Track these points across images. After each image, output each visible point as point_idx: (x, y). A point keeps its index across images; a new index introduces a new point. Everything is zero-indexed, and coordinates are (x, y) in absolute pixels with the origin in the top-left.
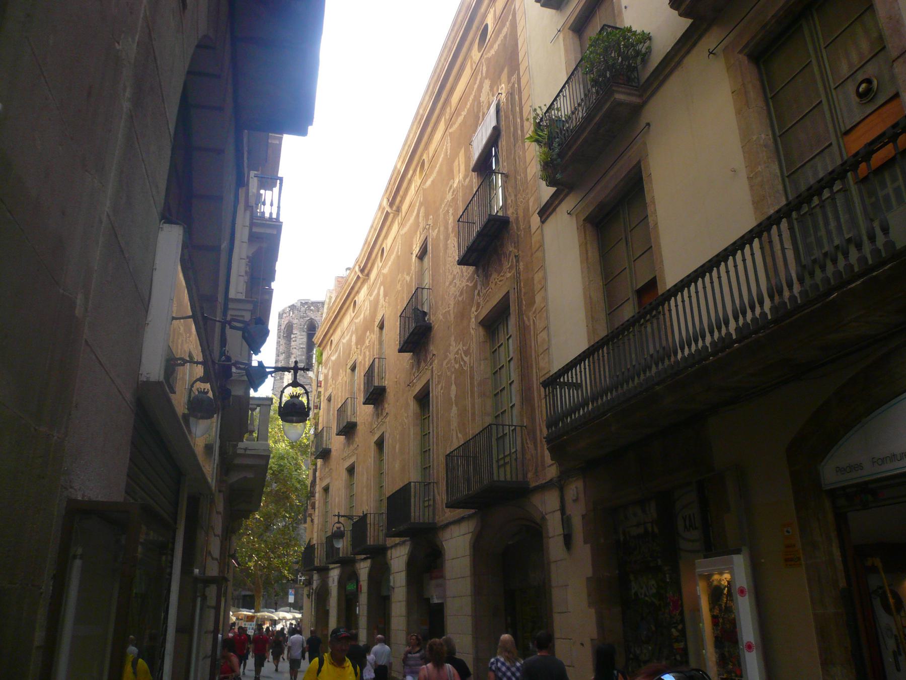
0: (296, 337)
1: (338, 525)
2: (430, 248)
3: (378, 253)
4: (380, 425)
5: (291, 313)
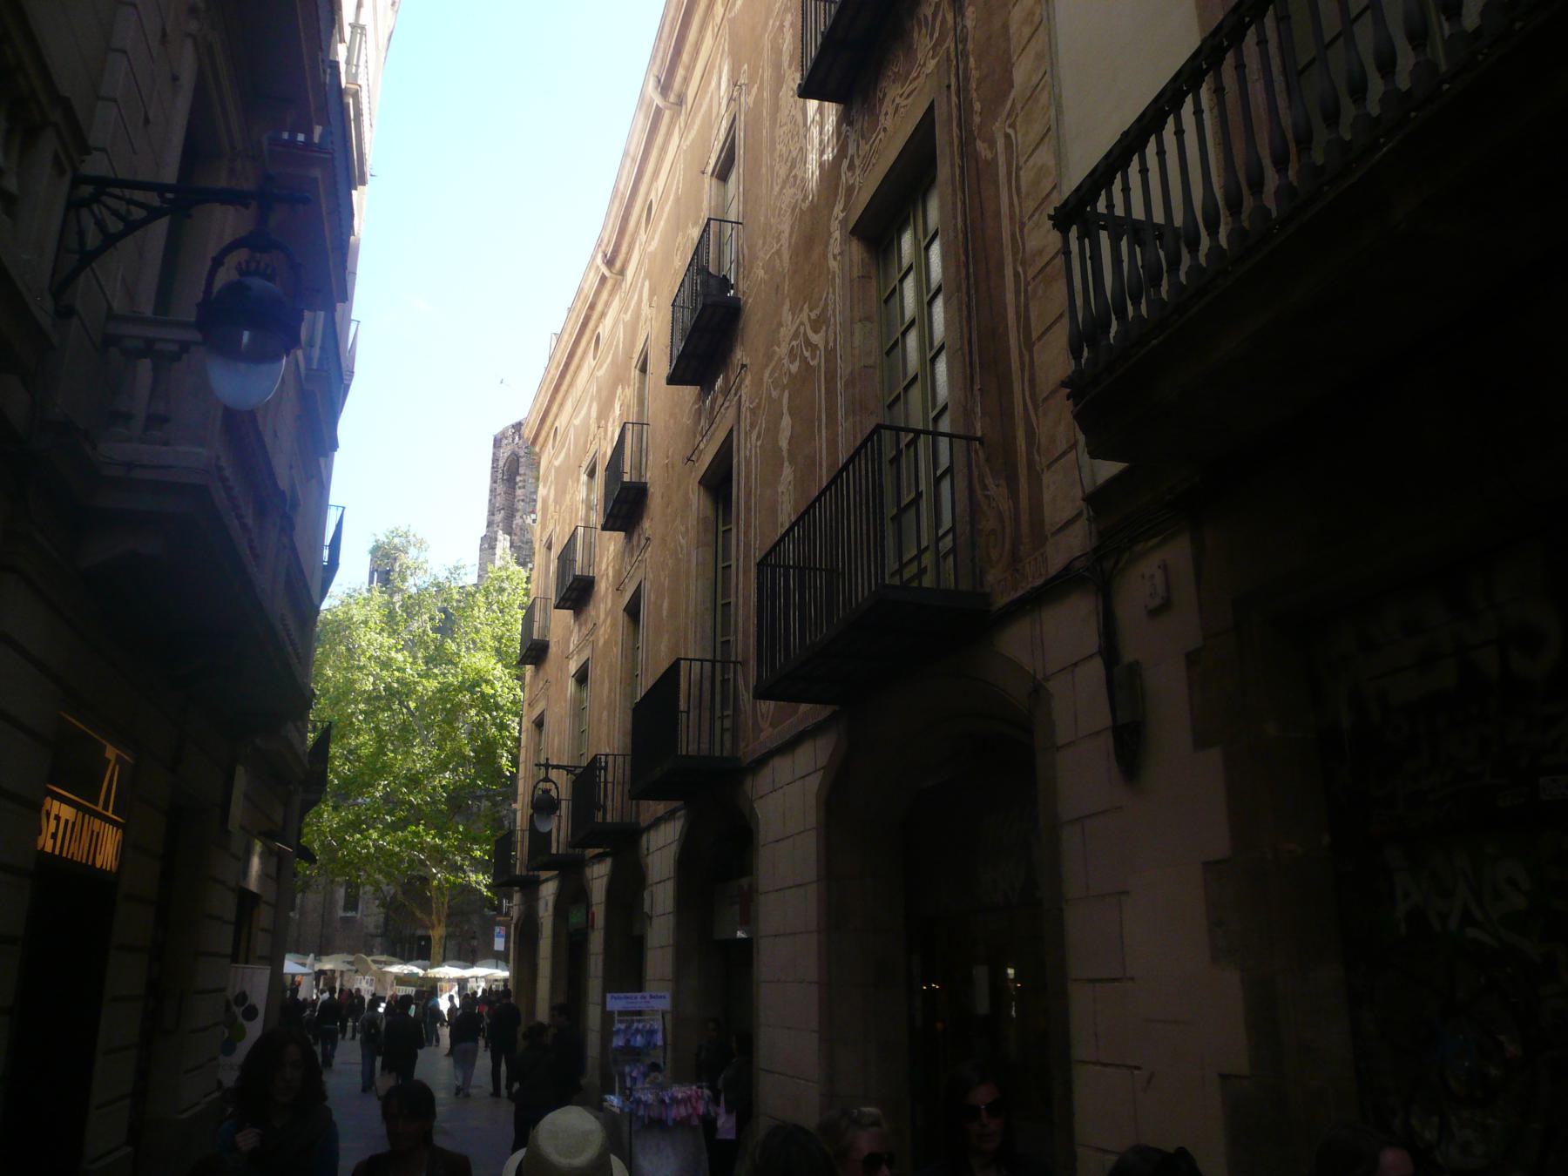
0: (524, 481)
1: (542, 785)
2: (740, 151)
3: (640, 217)
4: (635, 569)
5: (517, 437)
